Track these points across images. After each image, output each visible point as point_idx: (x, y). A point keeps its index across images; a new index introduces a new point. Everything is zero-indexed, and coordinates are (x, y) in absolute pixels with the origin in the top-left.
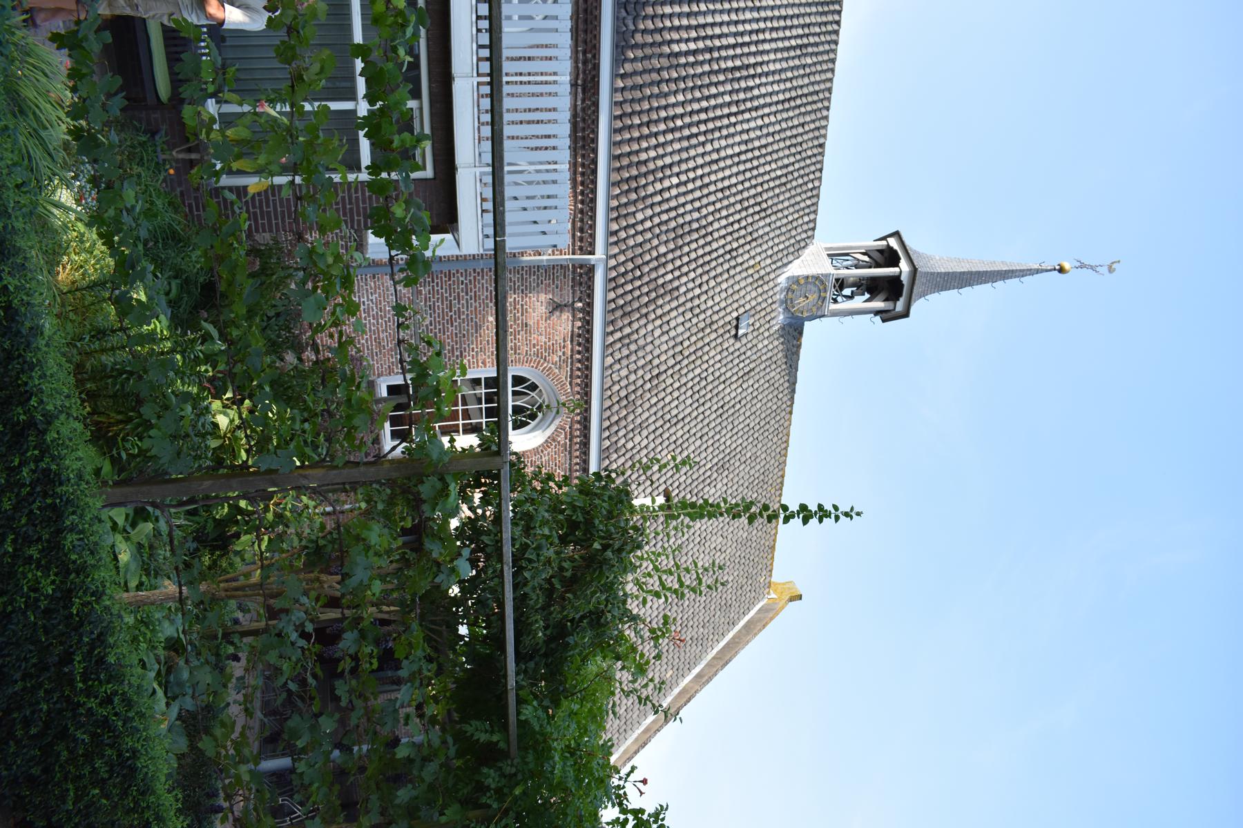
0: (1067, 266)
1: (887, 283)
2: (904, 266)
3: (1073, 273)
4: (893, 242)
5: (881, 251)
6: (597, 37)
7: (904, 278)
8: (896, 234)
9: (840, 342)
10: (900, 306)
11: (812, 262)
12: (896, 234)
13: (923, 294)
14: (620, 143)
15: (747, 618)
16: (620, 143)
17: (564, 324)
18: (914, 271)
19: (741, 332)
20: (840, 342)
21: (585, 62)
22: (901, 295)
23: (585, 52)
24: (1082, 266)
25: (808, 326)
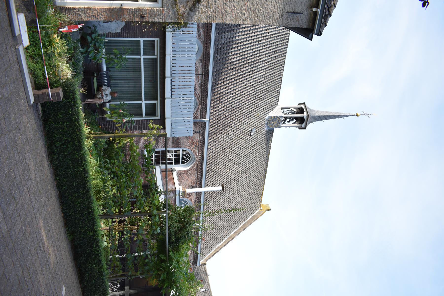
0: (359, 114)
1: (301, 117)
2: (305, 114)
4: (303, 106)
5: (299, 109)
7: (305, 118)
8: (304, 103)
9: (284, 135)
10: (303, 126)
11: (277, 112)
12: (304, 103)
15: (253, 215)
18: (308, 116)
19: (252, 134)
20: (284, 135)
21: (205, 69)
23: (205, 66)
24: (364, 114)
25: (276, 131)
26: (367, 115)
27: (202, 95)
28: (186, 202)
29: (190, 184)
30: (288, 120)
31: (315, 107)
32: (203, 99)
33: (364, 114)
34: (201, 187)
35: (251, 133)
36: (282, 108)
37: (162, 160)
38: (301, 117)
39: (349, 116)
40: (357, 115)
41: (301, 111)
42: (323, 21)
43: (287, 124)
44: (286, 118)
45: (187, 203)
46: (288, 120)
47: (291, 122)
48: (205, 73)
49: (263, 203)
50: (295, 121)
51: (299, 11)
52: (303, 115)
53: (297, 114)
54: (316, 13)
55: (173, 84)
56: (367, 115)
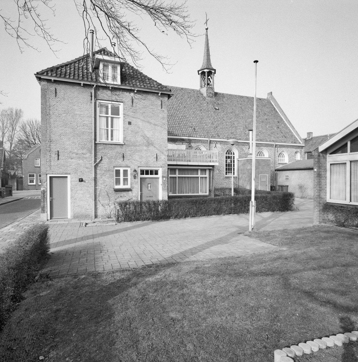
0: (206, 28)
1: (207, 73)
2: (205, 70)
3: (208, 26)
4: (200, 72)
5: (202, 75)
6: (176, 139)
7: (208, 70)
8: (198, 71)
9: (220, 84)
10: (213, 71)
11: (204, 91)
12: (198, 71)
13: (211, 65)
14: (91, 78)
15: (274, 106)
16: (91, 78)
17: (218, 145)
18: (207, 68)
19: (217, 108)
20: (220, 84)
21: (179, 141)
22: (211, 71)
23: (178, 141)
24: (206, 23)
25: (216, 90)
26: (207, 21)
27: (194, 143)
28: (258, 153)
29: (247, 150)
30: (209, 82)
31: (200, 64)
32: (196, 142)
33: (206, 23)
34: (127, 179)
35: (217, 109)
36: (201, 87)
37: (229, 166)
38: (207, 73)
39: (208, 50)
40: (207, 29)
41: (203, 73)
42: (164, 89)
43: (212, 83)
44: (208, 84)
45: (260, 152)
46: (209, 82)
47: (211, 80)
48: (182, 141)
49: (266, 98)
50: (209, 77)
51: (161, 102)
52: (206, 72)
53: (205, 76)
54: (161, 94)
55: (183, 160)
56: (207, 21)
